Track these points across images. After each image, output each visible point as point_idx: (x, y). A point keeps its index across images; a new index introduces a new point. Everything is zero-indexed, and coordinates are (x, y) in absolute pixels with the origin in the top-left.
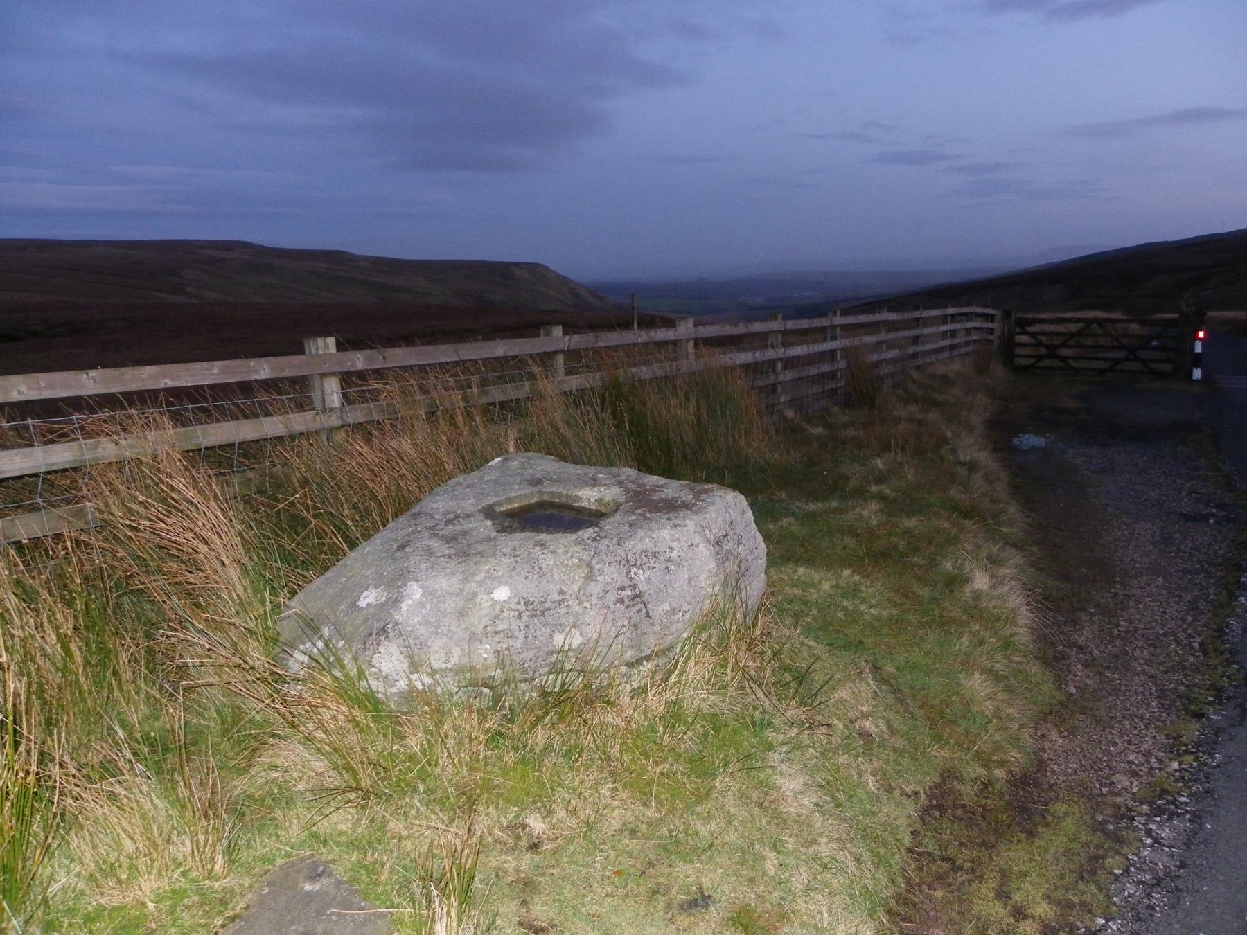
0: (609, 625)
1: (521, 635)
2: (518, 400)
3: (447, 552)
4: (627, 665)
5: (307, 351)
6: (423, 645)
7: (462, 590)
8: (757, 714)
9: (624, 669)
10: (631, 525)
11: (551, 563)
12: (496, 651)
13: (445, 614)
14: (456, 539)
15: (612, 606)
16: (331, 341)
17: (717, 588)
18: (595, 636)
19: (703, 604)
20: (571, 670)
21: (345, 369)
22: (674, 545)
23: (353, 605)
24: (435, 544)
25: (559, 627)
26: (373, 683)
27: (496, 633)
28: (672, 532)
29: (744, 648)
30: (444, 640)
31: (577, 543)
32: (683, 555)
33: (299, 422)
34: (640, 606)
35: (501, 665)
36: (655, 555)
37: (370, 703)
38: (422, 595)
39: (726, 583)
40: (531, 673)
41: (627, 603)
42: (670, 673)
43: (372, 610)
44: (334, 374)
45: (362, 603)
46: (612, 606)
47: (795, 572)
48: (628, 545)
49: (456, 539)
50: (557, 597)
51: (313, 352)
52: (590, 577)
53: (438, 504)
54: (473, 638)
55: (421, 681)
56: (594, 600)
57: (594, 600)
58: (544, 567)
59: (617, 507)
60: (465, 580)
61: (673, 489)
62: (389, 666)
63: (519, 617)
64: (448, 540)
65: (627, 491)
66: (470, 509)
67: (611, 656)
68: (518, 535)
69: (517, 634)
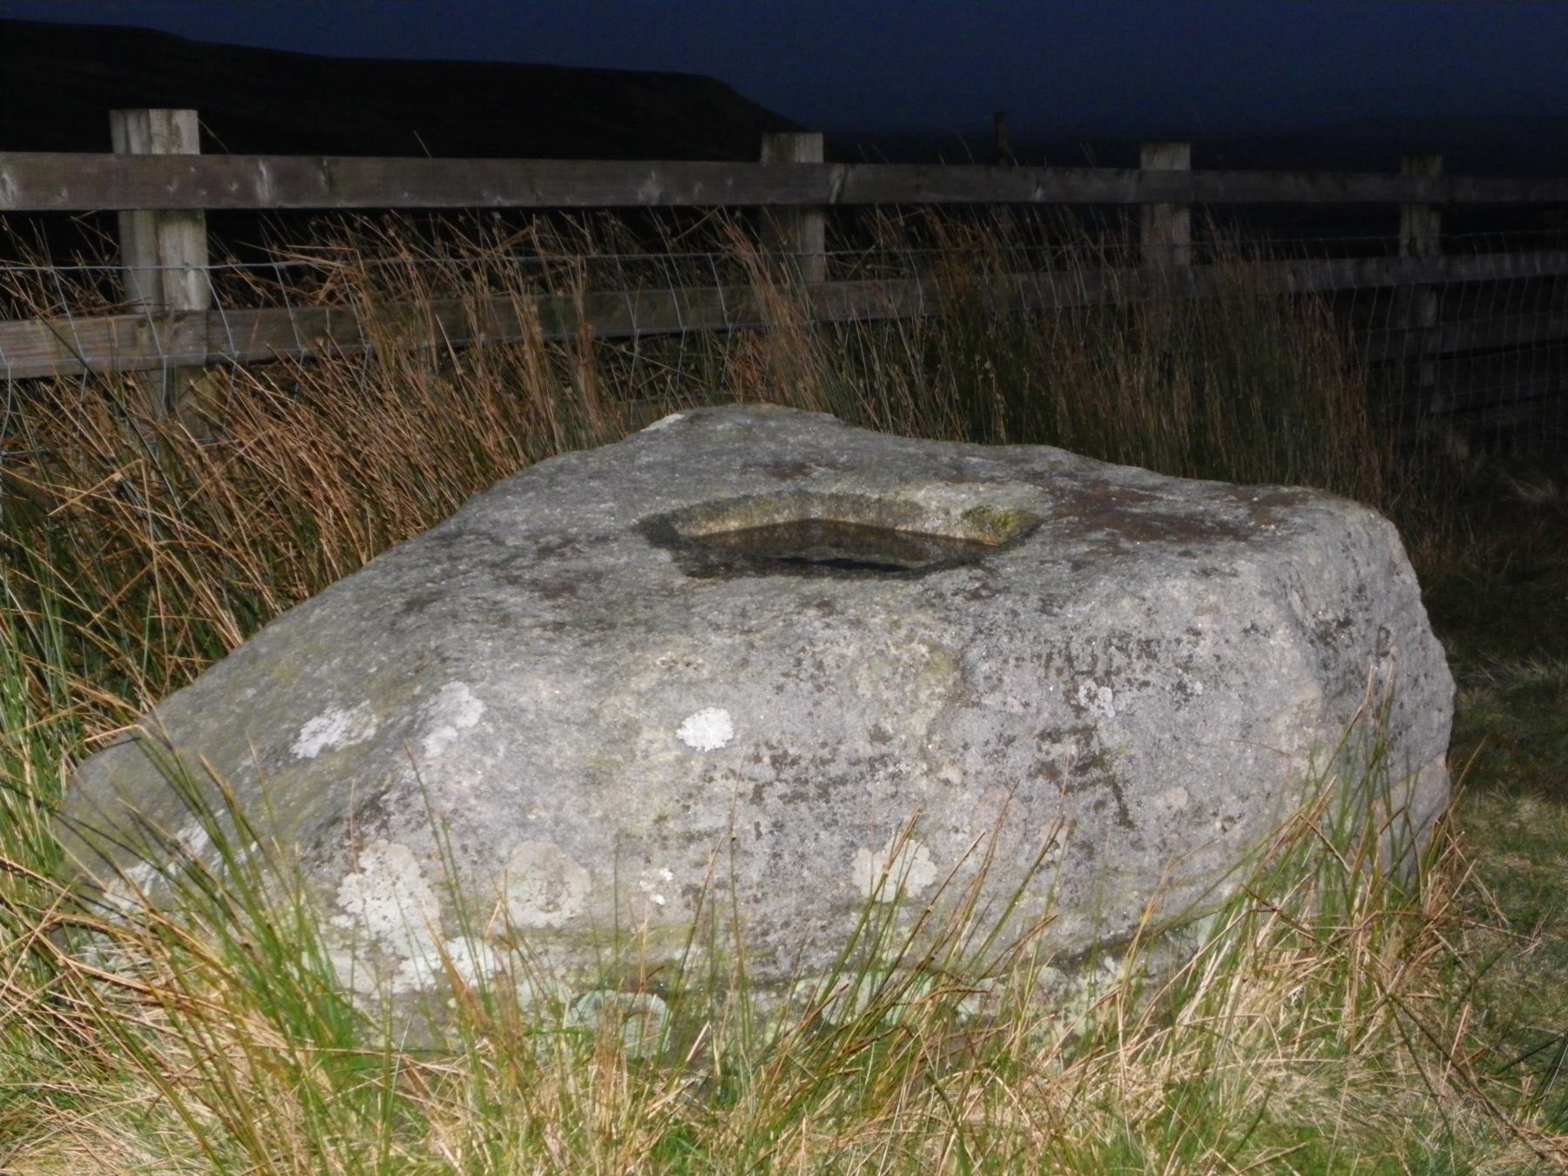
0: (1012, 837)
1: (762, 849)
2: (693, 338)
3: (549, 617)
4: (1057, 962)
5: (119, 146)
6: (485, 853)
7: (596, 715)
8: (1429, 1144)
9: (1048, 974)
10: (1077, 566)
11: (851, 652)
12: (690, 889)
13: (547, 775)
14: (571, 589)
15: (1025, 783)
16: (187, 122)
17: (1321, 761)
18: (972, 864)
19: (1281, 806)
20: (896, 965)
21: (224, 204)
22: (1203, 623)
23: (281, 753)
24: (512, 599)
25: (868, 834)
26: (342, 962)
27: (691, 838)
28: (1200, 587)
29: (1393, 946)
30: (545, 843)
31: (923, 604)
32: (1229, 653)
33: (94, 339)
34: (1102, 791)
35: (703, 931)
36: (1148, 648)
37: (320, 1017)
38: (485, 717)
39: (1344, 756)
40: (785, 964)
41: (1066, 777)
42: (1180, 997)
43: (337, 763)
44: (188, 214)
45: (308, 746)
46: (1025, 783)
47: (1509, 810)
48: (1070, 613)
49: (571, 589)
50: (866, 750)
51: (136, 149)
52: (962, 695)
53: (512, 513)
54: (626, 846)
55: (475, 962)
56: (973, 760)
57: (973, 760)
58: (829, 660)
59: (1029, 528)
60: (604, 687)
61: (1184, 496)
62: (385, 915)
63: (758, 796)
64: (549, 592)
65: (1055, 493)
66: (608, 523)
67: (1015, 926)
68: (750, 583)
69: (749, 844)
